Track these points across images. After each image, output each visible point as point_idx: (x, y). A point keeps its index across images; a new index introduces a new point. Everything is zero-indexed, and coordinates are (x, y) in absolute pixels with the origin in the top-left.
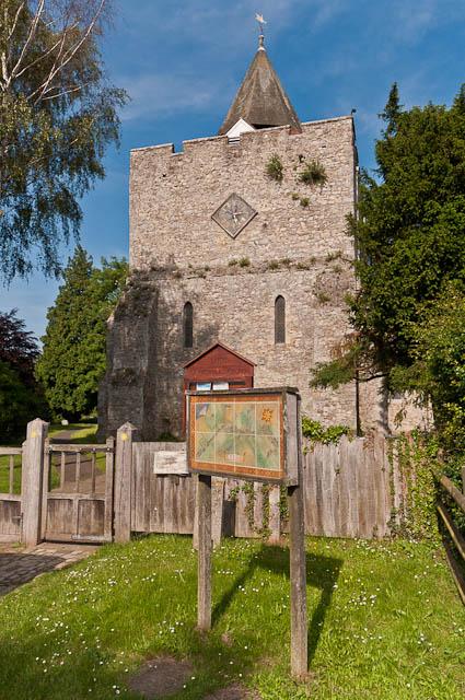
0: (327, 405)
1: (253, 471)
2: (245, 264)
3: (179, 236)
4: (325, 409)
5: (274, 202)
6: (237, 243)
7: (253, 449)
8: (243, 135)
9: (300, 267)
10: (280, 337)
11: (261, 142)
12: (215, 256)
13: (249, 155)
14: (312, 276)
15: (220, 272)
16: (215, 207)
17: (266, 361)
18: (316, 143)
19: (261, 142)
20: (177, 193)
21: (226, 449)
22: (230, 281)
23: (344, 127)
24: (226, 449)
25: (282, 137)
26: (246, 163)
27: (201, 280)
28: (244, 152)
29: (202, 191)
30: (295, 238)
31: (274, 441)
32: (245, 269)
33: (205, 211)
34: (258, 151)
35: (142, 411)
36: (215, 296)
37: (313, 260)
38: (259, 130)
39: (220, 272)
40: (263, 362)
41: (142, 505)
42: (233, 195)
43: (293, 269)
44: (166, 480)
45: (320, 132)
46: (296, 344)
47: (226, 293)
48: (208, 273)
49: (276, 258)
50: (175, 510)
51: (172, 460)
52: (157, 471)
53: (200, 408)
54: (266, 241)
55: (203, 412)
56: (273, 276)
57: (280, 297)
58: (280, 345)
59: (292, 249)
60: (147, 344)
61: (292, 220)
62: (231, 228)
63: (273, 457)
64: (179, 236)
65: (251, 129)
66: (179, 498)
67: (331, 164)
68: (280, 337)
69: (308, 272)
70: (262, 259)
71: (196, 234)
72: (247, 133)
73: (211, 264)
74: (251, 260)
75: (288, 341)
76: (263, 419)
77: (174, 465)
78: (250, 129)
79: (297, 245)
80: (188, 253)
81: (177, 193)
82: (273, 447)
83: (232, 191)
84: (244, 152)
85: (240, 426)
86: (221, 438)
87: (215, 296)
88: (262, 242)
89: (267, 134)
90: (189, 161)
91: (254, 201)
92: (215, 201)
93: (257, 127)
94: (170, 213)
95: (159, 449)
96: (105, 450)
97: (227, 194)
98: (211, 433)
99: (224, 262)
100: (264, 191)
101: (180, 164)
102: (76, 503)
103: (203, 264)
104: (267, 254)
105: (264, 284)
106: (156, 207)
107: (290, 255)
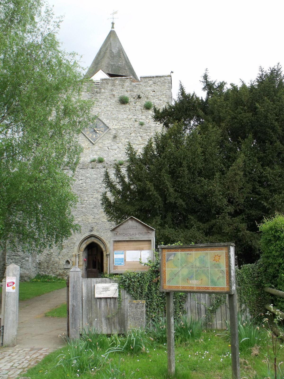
1: (208, 288)
2: (101, 161)
7: (208, 277)
8: (102, 80)
11: (113, 85)
13: (106, 92)
18: (149, 88)
19: (113, 85)
21: (189, 278)
23: (166, 81)
24: (189, 278)
25: (127, 83)
28: (103, 90)
31: (222, 272)
34: (112, 90)
36: (81, 182)
38: (113, 78)
44: (102, 300)
45: (151, 82)
51: (107, 289)
52: (97, 296)
53: (170, 255)
55: (172, 258)
61: (133, 134)
63: (221, 280)
65: (107, 77)
67: (158, 102)
70: (112, 159)
74: (105, 159)
76: (214, 260)
82: (221, 275)
84: (103, 90)
85: (198, 264)
86: (185, 272)
87: (81, 182)
89: (118, 80)
91: (108, 121)
93: (111, 75)
95: (97, 283)
98: (176, 269)
100: (115, 116)
104: (116, 156)
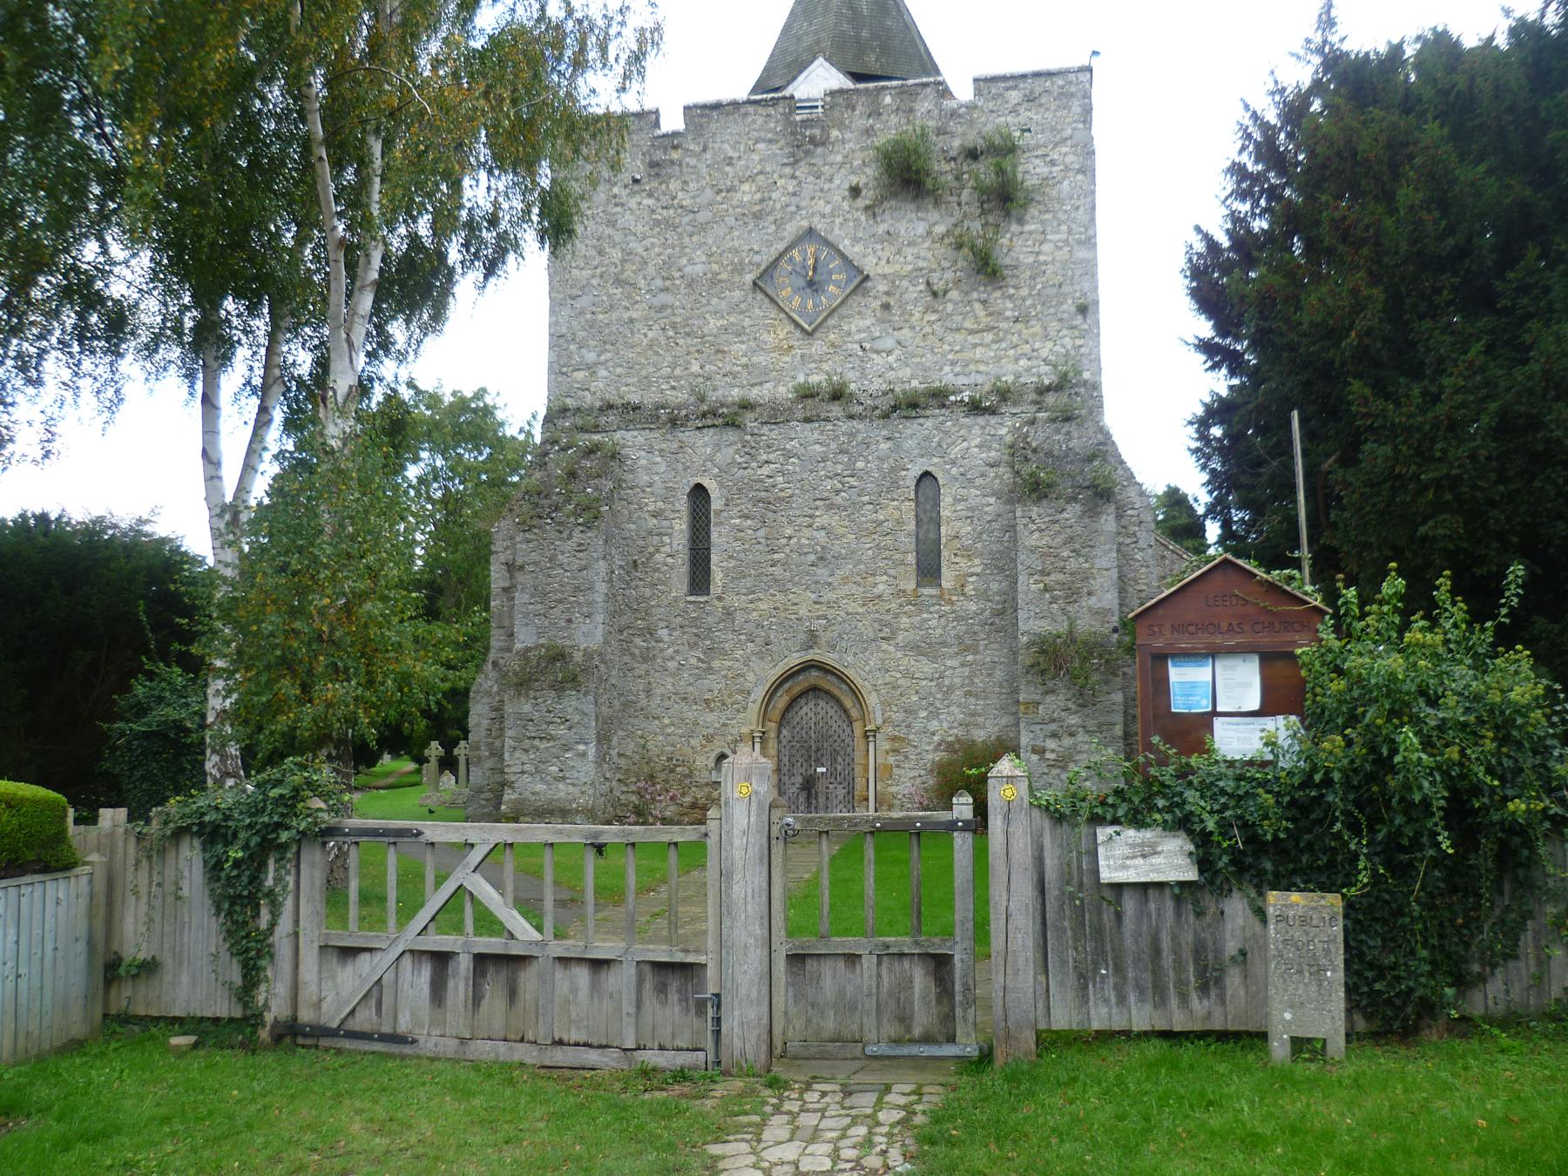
0: (1054, 735)
2: (837, 395)
3: (674, 326)
4: (1051, 744)
5: (909, 251)
6: (817, 347)
9: (975, 408)
10: (929, 570)
11: (875, 113)
12: (761, 375)
14: (1004, 427)
15: (776, 415)
16: (765, 259)
17: (894, 632)
20: (668, 224)
22: (805, 438)
26: (839, 158)
27: (731, 435)
28: (835, 133)
29: (731, 221)
30: (958, 337)
32: (836, 410)
33: (739, 269)
35: (592, 752)
37: (1004, 394)
39: (776, 415)
40: (886, 631)
41: (1063, 962)
42: (810, 232)
43: (959, 413)
46: (969, 589)
47: (793, 465)
48: (750, 415)
49: (915, 383)
50: (1157, 972)
54: (889, 343)
56: (915, 432)
57: (927, 474)
58: (927, 591)
59: (953, 363)
60: (602, 587)
62: (802, 311)
64: (674, 326)
65: (848, 84)
66: (1166, 944)
68: (929, 570)
69: (993, 420)
70: (877, 385)
71: (714, 323)
72: (841, 92)
73: (753, 394)
75: (948, 579)
77: (1155, 860)
78: (838, 80)
79: (967, 355)
80: (695, 368)
81: (668, 224)
83: (805, 223)
84: (835, 133)
87: (766, 470)
88: (881, 345)
90: (697, 149)
92: (760, 246)
93: (857, 77)
94: (651, 270)
96: (952, 826)
97: (791, 229)
99: (784, 392)
101: (675, 155)
102: (464, 964)
103: (736, 394)
105: (884, 446)
106: (616, 255)
107: (946, 377)
